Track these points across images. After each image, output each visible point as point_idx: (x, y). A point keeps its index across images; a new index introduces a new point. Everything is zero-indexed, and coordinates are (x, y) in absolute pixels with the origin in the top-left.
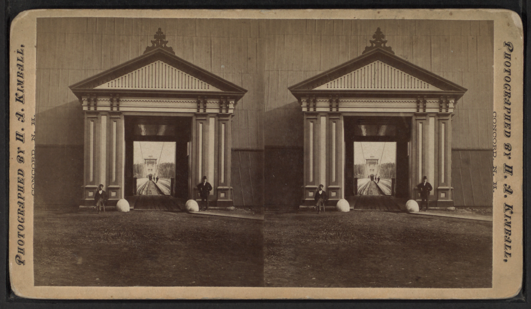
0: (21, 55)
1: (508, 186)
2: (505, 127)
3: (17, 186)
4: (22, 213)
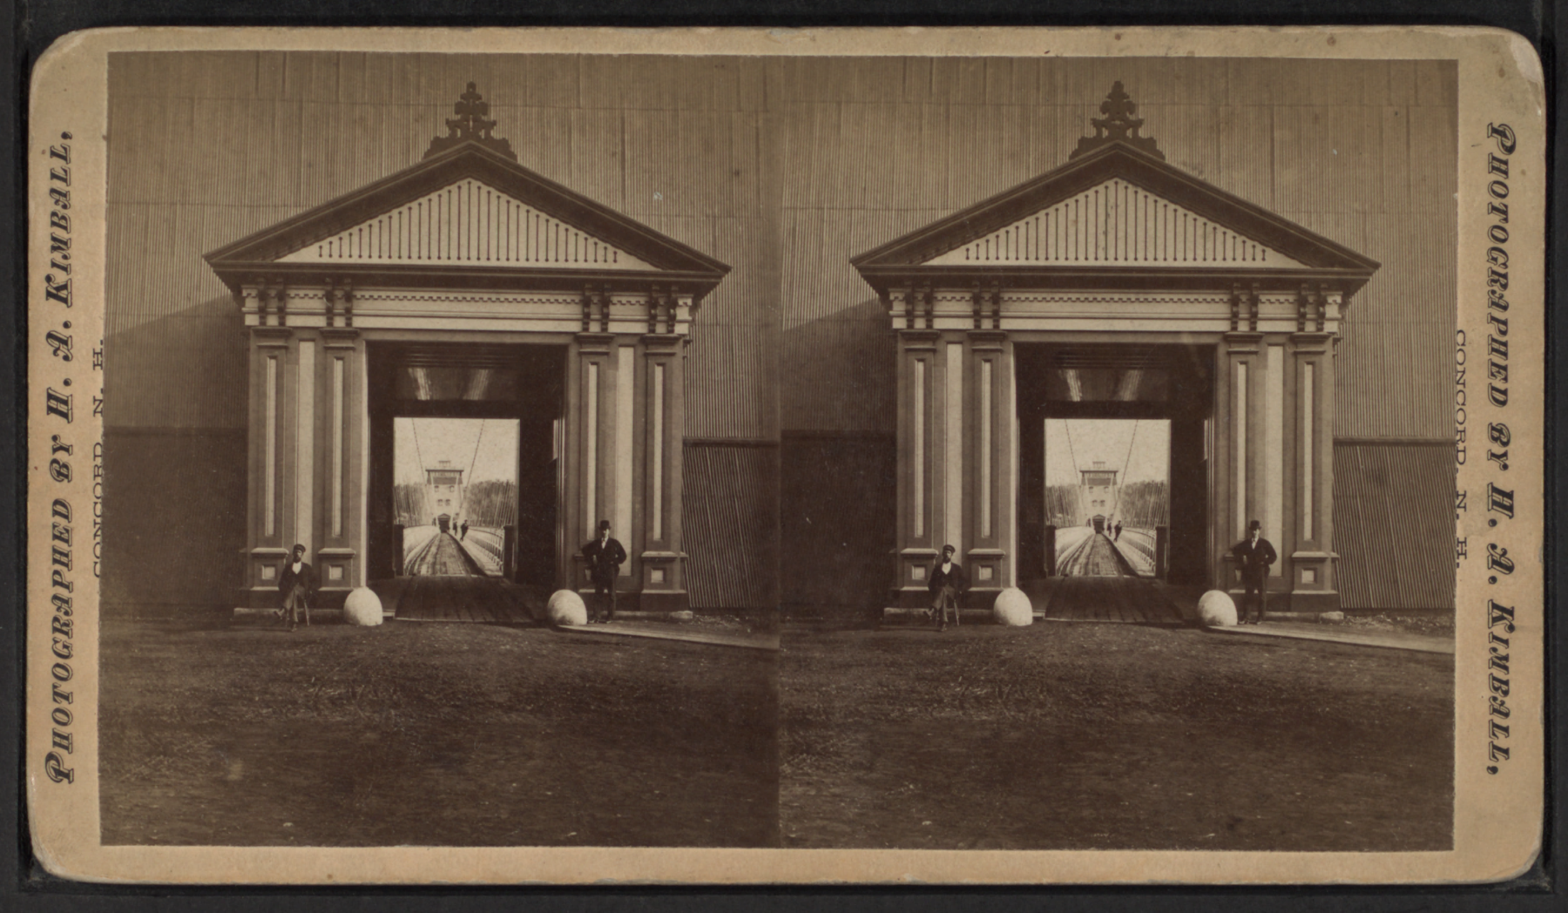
0: (61, 162)
1: (1499, 551)
2: (1493, 375)
3: (50, 551)
4: (65, 629)
